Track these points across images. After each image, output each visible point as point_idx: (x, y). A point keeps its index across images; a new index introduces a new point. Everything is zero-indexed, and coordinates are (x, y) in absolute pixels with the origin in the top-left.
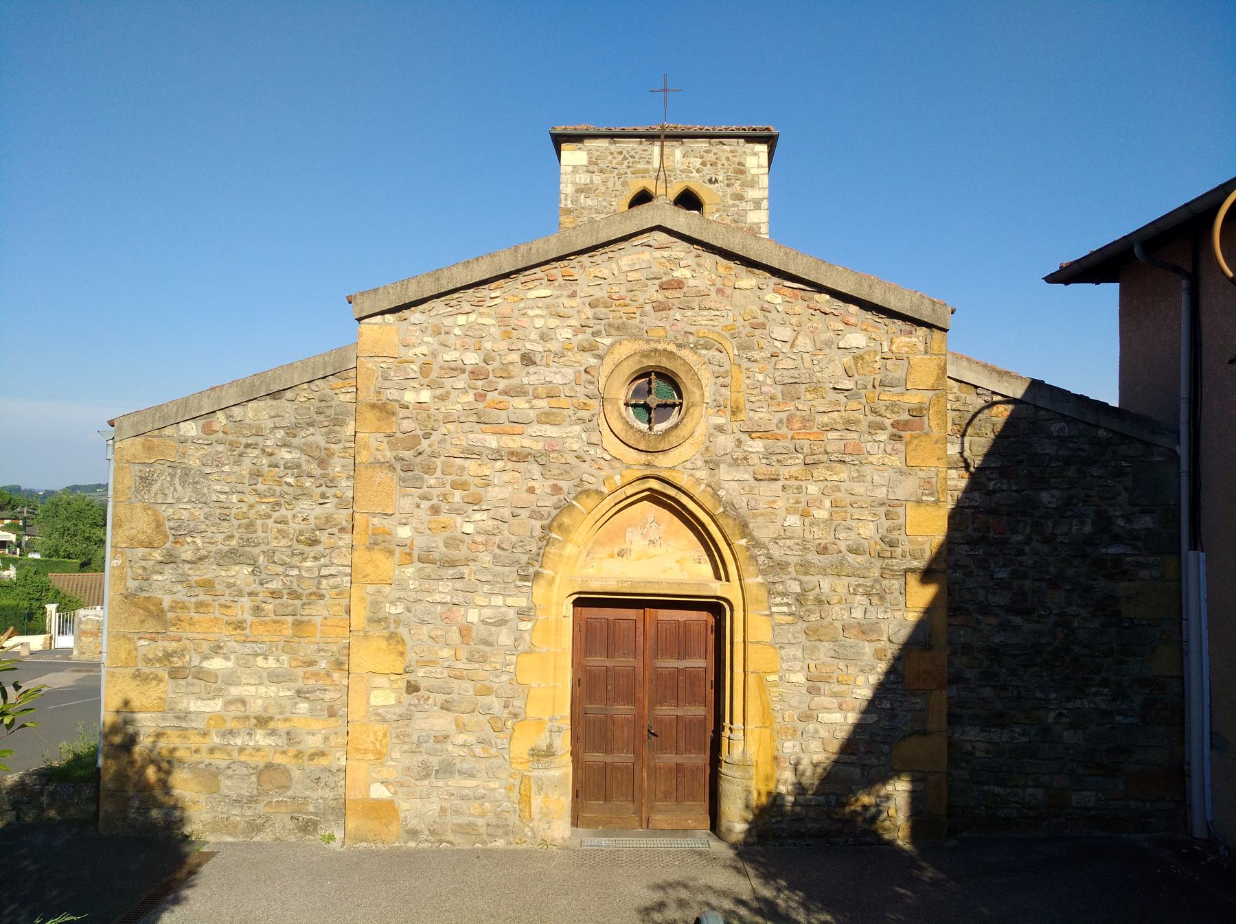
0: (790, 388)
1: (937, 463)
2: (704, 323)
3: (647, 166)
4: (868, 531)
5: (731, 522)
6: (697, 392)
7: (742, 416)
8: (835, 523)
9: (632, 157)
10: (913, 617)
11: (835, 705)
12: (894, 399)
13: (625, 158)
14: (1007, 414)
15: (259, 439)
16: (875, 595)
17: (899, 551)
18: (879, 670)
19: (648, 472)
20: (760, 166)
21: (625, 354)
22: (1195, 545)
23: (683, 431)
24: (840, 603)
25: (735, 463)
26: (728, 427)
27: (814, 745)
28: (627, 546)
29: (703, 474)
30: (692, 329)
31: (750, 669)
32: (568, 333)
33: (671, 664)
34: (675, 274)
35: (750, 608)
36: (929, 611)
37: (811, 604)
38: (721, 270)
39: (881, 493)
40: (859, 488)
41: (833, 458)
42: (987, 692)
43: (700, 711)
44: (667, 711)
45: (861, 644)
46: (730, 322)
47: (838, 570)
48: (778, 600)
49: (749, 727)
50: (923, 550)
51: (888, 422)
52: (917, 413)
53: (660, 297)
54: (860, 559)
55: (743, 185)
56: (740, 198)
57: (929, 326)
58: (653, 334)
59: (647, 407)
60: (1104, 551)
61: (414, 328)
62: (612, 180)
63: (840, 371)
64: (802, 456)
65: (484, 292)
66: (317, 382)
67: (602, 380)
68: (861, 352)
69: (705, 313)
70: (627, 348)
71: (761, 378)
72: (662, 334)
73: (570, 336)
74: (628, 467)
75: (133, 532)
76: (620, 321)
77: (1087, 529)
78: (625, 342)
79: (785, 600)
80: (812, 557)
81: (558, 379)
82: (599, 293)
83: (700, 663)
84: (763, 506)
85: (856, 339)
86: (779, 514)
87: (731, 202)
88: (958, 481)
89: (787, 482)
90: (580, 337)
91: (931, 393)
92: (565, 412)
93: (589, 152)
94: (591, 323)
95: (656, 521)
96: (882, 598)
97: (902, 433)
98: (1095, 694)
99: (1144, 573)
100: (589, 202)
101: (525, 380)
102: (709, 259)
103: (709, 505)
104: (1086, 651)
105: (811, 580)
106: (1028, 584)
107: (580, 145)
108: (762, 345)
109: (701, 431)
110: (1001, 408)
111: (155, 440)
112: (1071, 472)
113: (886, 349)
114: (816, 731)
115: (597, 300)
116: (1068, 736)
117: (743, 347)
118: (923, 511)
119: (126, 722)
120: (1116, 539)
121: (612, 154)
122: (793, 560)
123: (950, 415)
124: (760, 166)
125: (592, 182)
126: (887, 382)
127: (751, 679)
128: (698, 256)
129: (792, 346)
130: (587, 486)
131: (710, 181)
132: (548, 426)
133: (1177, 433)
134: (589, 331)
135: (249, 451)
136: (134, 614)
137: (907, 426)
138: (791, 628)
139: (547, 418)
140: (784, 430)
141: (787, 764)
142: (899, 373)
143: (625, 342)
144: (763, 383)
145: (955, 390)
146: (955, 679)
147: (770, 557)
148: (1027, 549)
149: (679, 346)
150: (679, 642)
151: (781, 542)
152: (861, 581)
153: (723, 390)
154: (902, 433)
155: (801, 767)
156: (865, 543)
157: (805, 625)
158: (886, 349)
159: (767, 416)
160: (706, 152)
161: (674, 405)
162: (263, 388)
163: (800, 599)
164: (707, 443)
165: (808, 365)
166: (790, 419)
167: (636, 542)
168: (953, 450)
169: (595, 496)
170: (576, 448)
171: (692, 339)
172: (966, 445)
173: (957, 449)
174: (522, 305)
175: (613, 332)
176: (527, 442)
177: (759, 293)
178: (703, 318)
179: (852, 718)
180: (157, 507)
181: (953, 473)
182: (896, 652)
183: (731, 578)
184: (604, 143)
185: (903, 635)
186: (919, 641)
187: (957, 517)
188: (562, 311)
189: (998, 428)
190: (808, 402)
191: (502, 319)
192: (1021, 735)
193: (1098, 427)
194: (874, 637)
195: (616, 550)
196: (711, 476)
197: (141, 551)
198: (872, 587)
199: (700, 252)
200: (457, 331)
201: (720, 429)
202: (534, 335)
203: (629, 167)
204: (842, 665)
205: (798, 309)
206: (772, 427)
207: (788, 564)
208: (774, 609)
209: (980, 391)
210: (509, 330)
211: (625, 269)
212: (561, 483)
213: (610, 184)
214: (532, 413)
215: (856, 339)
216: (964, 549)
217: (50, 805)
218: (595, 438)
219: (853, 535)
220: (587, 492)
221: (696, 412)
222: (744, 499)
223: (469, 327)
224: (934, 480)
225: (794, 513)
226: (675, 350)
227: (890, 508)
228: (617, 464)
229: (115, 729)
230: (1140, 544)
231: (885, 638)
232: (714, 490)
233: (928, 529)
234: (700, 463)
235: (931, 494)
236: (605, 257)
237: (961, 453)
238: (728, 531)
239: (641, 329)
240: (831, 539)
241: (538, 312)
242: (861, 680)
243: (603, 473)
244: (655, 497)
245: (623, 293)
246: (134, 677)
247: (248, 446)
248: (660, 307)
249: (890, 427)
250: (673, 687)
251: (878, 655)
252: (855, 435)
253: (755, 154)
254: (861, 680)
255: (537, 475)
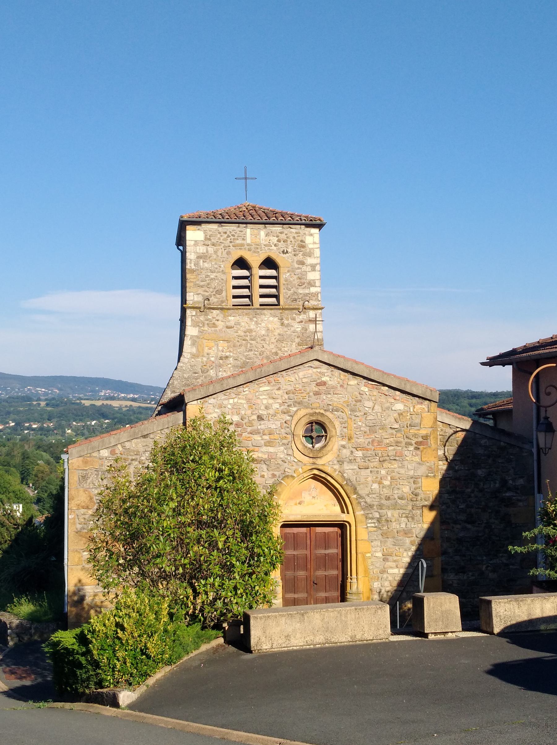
0: (372, 429)
1: (434, 460)
2: (336, 400)
3: (243, 242)
4: (406, 489)
5: (350, 488)
6: (334, 431)
7: (353, 441)
8: (393, 486)
9: (233, 235)
10: (426, 526)
11: (395, 566)
12: (416, 432)
13: (228, 236)
14: (463, 436)
15: (138, 457)
16: (410, 517)
17: (419, 498)
18: (412, 550)
19: (313, 467)
20: (314, 243)
21: (302, 415)
22: (539, 492)
23: (328, 448)
24: (395, 521)
25: (350, 461)
26: (347, 446)
27: (387, 584)
28: (303, 499)
29: (337, 467)
30: (330, 403)
31: (359, 551)
32: (276, 406)
33: (323, 552)
34: (323, 379)
35: (358, 525)
36: (433, 523)
37: (383, 522)
38: (342, 377)
39: (411, 473)
40: (402, 471)
41: (391, 458)
42: (457, 558)
43: (335, 572)
44: (321, 573)
45: (405, 539)
46: (347, 399)
47: (395, 507)
48: (370, 521)
49: (359, 577)
50: (429, 497)
51: (413, 442)
52: (426, 437)
53: (316, 389)
54: (403, 502)
55: (304, 255)
56: (302, 263)
57: (430, 400)
58: (314, 406)
59: (311, 437)
60: (504, 495)
61: (210, 405)
62: (220, 251)
63: (393, 420)
64: (378, 458)
65: (241, 389)
66: (165, 430)
67: (293, 426)
68: (402, 412)
69: (336, 396)
70: (303, 412)
71: (360, 424)
72: (318, 405)
73: (278, 407)
74: (305, 465)
75: (79, 502)
76: (299, 400)
77: (497, 485)
78: (302, 410)
79: (373, 521)
80: (384, 502)
81: (273, 426)
82: (290, 388)
83: (335, 551)
84: (363, 480)
85: (399, 406)
86: (369, 484)
87: (297, 266)
88: (443, 466)
89: (372, 469)
90: (282, 407)
91: (431, 429)
92: (277, 441)
93: (205, 232)
94: (287, 401)
95: (315, 488)
96: (413, 518)
97: (420, 447)
98: (502, 557)
99: (521, 504)
100: (206, 265)
101: (259, 427)
102: (337, 372)
103: (340, 480)
104: (498, 538)
105: (383, 512)
106: (473, 510)
107: (199, 227)
108: (360, 409)
109: (336, 448)
110: (460, 433)
111: (88, 458)
112: (490, 461)
113: (412, 410)
114: (388, 578)
115: (290, 391)
116: (491, 575)
117: (352, 410)
118: (430, 480)
119: (79, 590)
120: (509, 489)
121: (220, 233)
122: (376, 503)
123: (439, 437)
124: (314, 243)
125: (207, 251)
126: (413, 424)
127: (360, 556)
128: (332, 371)
129: (373, 409)
130: (287, 474)
131: (283, 252)
132: (269, 447)
133: (532, 443)
134: (286, 404)
135: (133, 462)
136: (81, 540)
137: (421, 444)
138: (376, 533)
139: (269, 444)
140: (370, 446)
141: (375, 592)
142: (417, 421)
143: (302, 410)
144: (362, 426)
145: (441, 426)
146: (444, 553)
147: (366, 502)
148: (473, 495)
149: (325, 410)
150: (325, 541)
151: (370, 496)
152: (404, 511)
153: (345, 429)
154: (420, 447)
155: (381, 593)
156: (405, 494)
157: (382, 531)
158: (412, 410)
159: (363, 440)
160: (281, 233)
161: (323, 436)
162: (140, 433)
163: (379, 520)
164: (338, 453)
165: (380, 418)
166: (373, 441)
167: (306, 497)
168: (440, 453)
169: (291, 478)
170: (282, 456)
171: (331, 407)
172: (446, 450)
173: (442, 452)
174: (257, 394)
175: (297, 405)
176: (260, 455)
177: (358, 387)
178: (335, 398)
179: (402, 571)
180: (90, 490)
181: (441, 463)
182: (420, 542)
183: (350, 512)
184: (214, 226)
185: (422, 534)
186: (429, 536)
187: (443, 482)
188: (274, 396)
189: (459, 442)
190: (380, 434)
191: (249, 401)
192: (472, 576)
193: (500, 441)
194: (410, 535)
195: (298, 502)
196: (340, 467)
197: (82, 511)
198: (409, 514)
199: (333, 369)
200: (229, 406)
201: (344, 447)
202: (263, 408)
203: (231, 242)
204: (397, 548)
205: (375, 393)
206: (365, 445)
207: (373, 505)
208: (369, 525)
209: (451, 426)
210: (252, 405)
211: (301, 377)
212: (276, 473)
213: (219, 253)
214: (263, 442)
215: (399, 406)
216: (446, 496)
217: (35, 634)
218: (290, 452)
219: (400, 492)
220: (287, 476)
221: (333, 439)
222: (355, 477)
223: (234, 404)
224: (433, 467)
225: (376, 483)
226: (324, 413)
227: (415, 479)
228: (300, 464)
229: (74, 593)
230: (519, 492)
231: (415, 536)
232: (342, 473)
233: (431, 488)
234: (336, 462)
235: (432, 473)
236: (292, 372)
237: (444, 454)
238: (348, 492)
239: (309, 403)
240: (391, 493)
241: (264, 397)
242: (405, 554)
243: (294, 468)
244: (315, 478)
245: (301, 388)
246: (82, 569)
247: (132, 460)
248: (317, 394)
249: (414, 444)
250: (324, 562)
251: (412, 543)
252: (400, 448)
253: (311, 235)
254: (405, 554)
255: (265, 470)
